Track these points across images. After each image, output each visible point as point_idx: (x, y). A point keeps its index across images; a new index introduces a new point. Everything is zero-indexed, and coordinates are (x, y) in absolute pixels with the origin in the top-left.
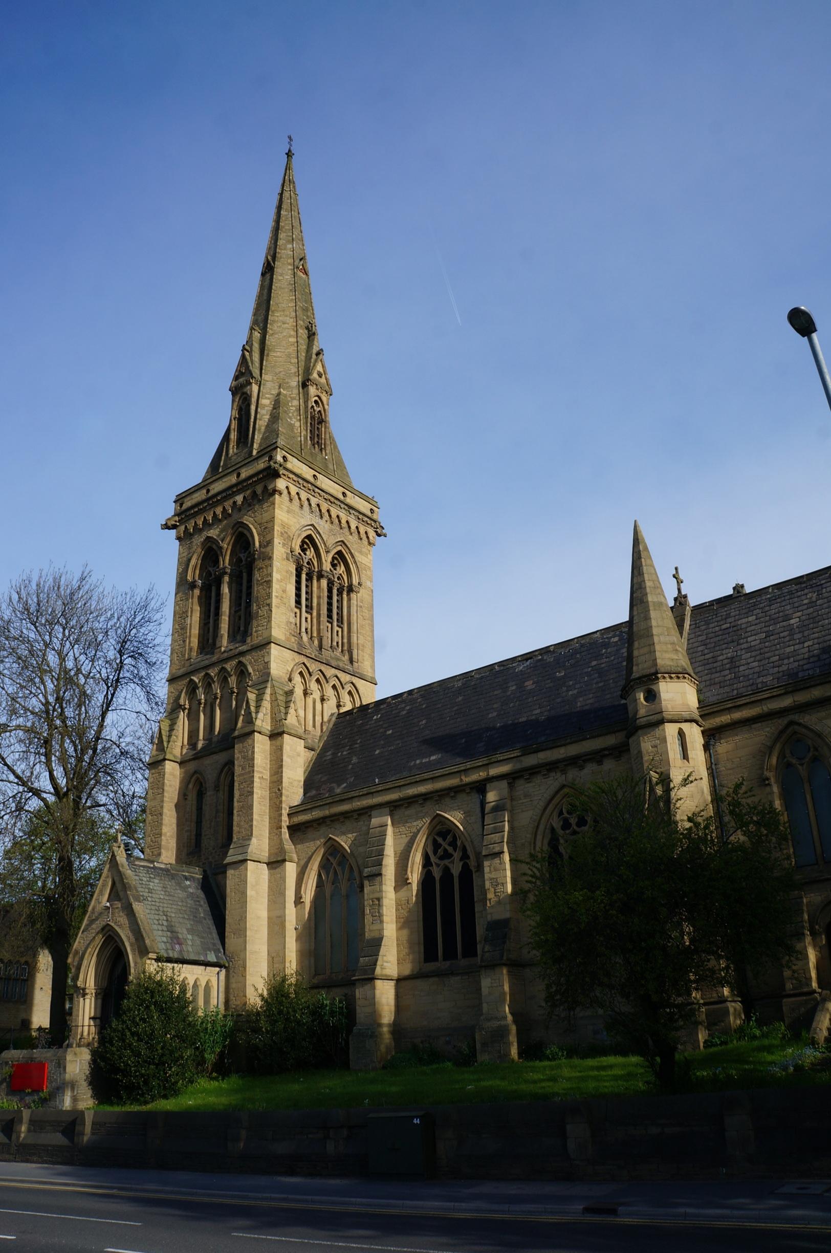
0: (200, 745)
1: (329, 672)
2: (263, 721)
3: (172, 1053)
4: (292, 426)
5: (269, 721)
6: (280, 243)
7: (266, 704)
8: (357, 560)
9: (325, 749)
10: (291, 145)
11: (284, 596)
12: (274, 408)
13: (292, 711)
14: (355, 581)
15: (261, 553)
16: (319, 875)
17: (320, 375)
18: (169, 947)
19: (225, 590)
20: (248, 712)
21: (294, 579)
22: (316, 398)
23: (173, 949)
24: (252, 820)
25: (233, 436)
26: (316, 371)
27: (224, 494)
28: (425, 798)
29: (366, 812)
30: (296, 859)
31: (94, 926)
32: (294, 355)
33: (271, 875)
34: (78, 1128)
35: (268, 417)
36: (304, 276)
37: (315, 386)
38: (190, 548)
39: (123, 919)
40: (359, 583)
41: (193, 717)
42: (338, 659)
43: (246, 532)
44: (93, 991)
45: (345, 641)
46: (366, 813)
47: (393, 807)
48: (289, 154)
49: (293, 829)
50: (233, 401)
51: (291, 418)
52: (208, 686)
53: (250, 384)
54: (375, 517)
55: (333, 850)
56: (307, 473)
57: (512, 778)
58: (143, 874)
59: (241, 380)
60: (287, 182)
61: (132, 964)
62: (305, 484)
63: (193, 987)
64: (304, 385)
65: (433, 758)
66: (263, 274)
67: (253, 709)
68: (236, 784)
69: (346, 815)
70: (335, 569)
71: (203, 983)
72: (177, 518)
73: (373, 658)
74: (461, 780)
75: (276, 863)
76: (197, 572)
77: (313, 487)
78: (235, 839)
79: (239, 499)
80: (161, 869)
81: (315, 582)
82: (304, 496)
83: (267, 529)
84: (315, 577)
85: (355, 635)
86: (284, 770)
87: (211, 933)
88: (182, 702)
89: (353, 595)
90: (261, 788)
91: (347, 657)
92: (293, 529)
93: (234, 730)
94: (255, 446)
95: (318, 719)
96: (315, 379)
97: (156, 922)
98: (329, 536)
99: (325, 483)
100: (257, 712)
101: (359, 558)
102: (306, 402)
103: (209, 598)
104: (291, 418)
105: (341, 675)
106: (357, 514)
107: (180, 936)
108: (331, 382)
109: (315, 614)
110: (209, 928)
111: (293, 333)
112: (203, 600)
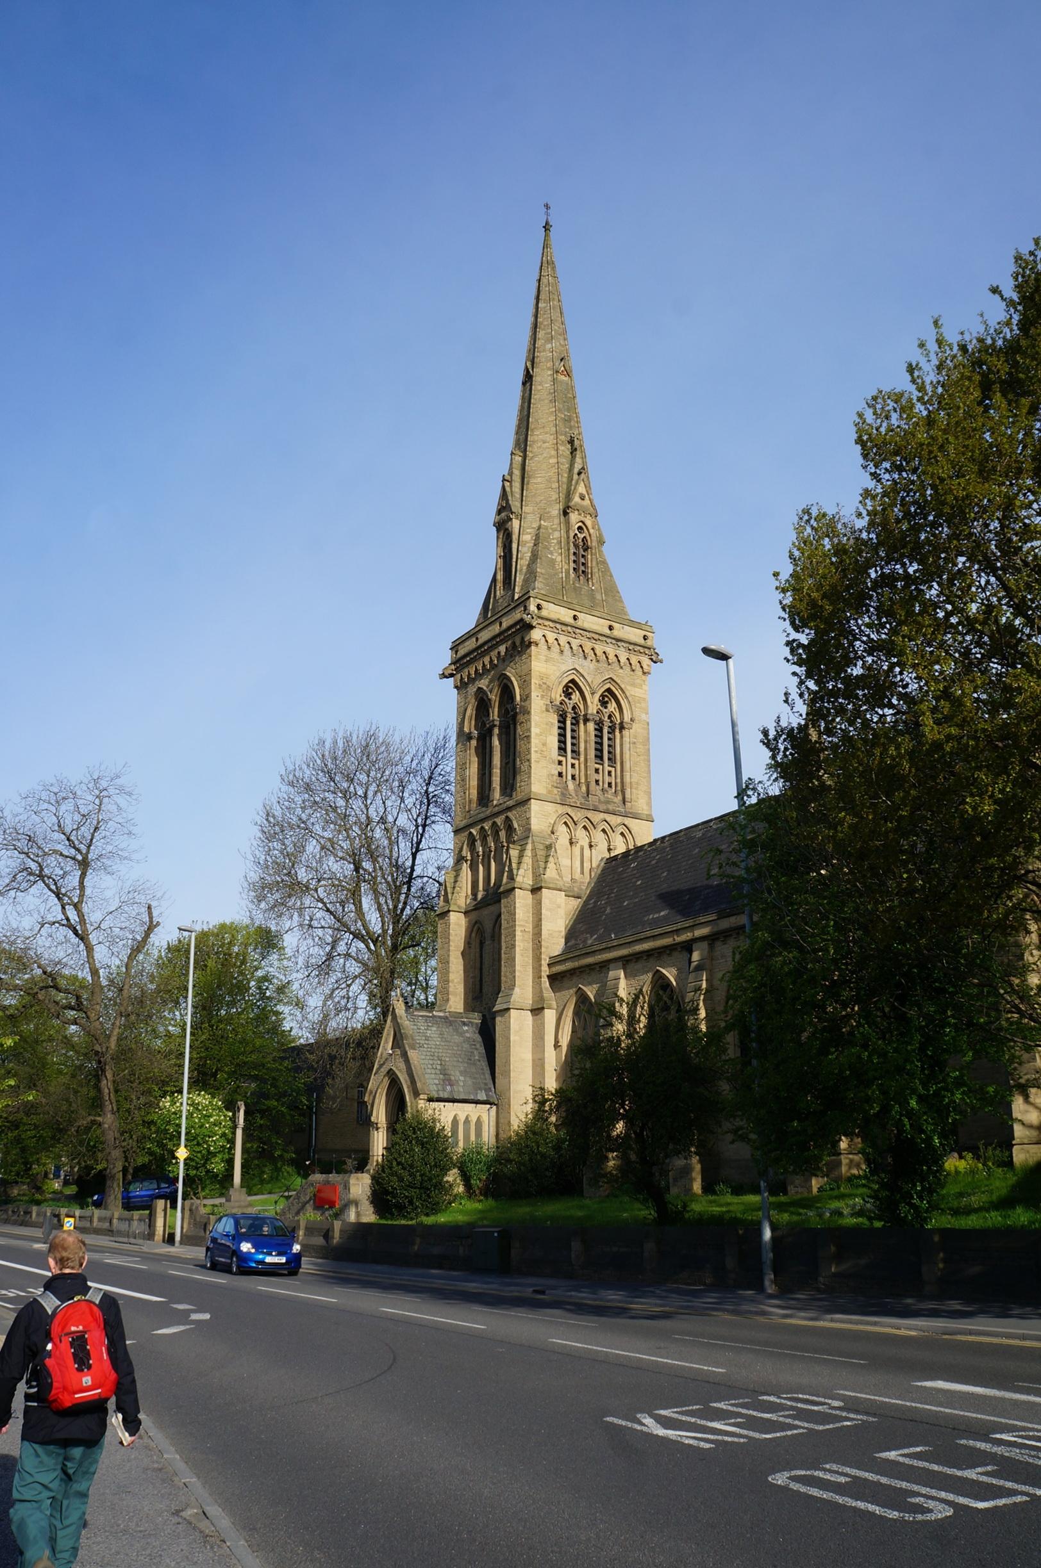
0: (480, 896)
1: (597, 817)
2: (524, 877)
3: (430, 1179)
4: (553, 562)
5: (531, 876)
6: (539, 343)
7: (528, 860)
8: (628, 695)
9: (590, 897)
10: (548, 215)
11: (544, 749)
12: (535, 545)
13: (551, 865)
14: (627, 719)
15: (522, 707)
16: (574, 1022)
17: (582, 498)
18: (440, 1087)
19: (496, 742)
20: (511, 870)
21: (556, 731)
22: (580, 524)
23: (444, 1090)
24: (514, 971)
25: (500, 577)
26: (578, 494)
27: (490, 644)
28: (649, 954)
29: (604, 966)
30: (554, 1004)
31: (382, 1070)
32: (555, 479)
33: (534, 1020)
34: (330, 1233)
35: (529, 554)
36: (566, 379)
37: (576, 512)
38: (466, 698)
39: (402, 1065)
40: (632, 720)
41: (474, 868)
42: (608, 802)
43: (509, 684)
44: (385, 1126)
45: (619, 780)
46: (605, 966)
47: (626, 962)
48: (547, 227)
49: (552, 978)
50: (498, 537)
51: (552, 553)
52: (484, 838)
53: (511, 519)
54: (649, 643)
55: (582, 998)
56: (565, 615)
57: (711, 939)
58: (422, 1025)
59: (503, 514)
60: (546, 264)
61: (409, 1104)
62: (564, 628)
63: (464, 1122)
64: (565, 513)
65: (662, 914)
66: (524, 384)
67: (514, 866)
68: (503, 937)
69: (590, 967)
70: (606, 708)
71: (474, 1119)
72: (453, 667)
73: (649, 794)
74: (674, 940)
75: (537, 1011)
76: (473, 722)
77: (573, 628)
78: (503, 989)
79: (502, 649)
80: (440, 1017)
81: (582, 725)
82: (563, 640)
83: (526, 683)
84: (581, 722)
85: (628, 774)
86: (543, 922)
87: (484, 1074)
88: (464, 853)
89: (626, 732)
90: (523, 940)
91: (620, 797)
92: (553, 678)
93: (500, 886)
94: (517, 589)
95: (587, 865)
96: (577, 504)
97: (430, 1066)
98: (593, 677)
99: (588, 621)
100: (518, 869)
101: (631, 691)
102: (568, 532)
103: (484, 747)
104: (552, 553)
105: (609, 817)
106: (625, 645)
107: (453, 1078)
108: (595, 502)
109: (582, 759)
110: (482, 1069)
111: (553, 453)
112: (480, 751)
